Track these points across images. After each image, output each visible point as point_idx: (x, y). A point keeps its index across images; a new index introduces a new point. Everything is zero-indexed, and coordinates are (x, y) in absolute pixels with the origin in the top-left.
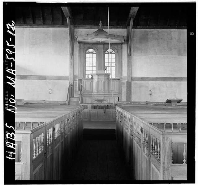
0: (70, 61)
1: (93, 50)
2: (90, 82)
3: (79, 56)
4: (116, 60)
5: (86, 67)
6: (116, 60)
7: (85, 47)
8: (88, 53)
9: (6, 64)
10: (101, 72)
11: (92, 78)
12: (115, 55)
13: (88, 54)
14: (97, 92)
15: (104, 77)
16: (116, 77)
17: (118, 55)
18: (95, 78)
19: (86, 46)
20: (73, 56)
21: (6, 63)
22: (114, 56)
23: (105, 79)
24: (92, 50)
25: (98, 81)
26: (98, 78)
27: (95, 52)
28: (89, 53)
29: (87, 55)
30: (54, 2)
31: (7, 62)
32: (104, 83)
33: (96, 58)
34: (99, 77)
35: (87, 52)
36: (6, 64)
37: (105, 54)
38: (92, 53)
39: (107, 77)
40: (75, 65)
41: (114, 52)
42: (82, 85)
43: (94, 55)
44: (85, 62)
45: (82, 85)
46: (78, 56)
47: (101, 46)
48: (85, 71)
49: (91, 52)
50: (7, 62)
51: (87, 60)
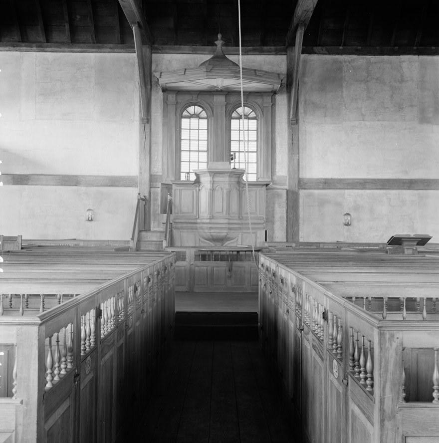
1: (201, 109)
3: (163, 125)
4: (259, 133)
7: (179, 101)
8: (186, 117)
10: (220, 166)
11: (197, 182)
12: (255, 121)
16: (260, 180)
18: (206, 180)
19: (183, 99)
20: (147, 126)
22: (253, 124)
24: (198, 109)
25: (213, 190)
26: (213, 183)
27: (204, 114)
28: (191, 116)
29: (185, 122)
32: (229, 193)
33: (208, 129)
34: (216, 179)
35: (185, 113)
37: (232, 118)
38: (197, 116)
39: (236, 180)
41: (253, 115)
42: (171, 200)
43: (204, 123)
44: (179, 139)
45: (171, 200)
46: (161, 124)
47: (221, 99)
48: (180, 132)
49: (195, 114)
51: (185, 134)
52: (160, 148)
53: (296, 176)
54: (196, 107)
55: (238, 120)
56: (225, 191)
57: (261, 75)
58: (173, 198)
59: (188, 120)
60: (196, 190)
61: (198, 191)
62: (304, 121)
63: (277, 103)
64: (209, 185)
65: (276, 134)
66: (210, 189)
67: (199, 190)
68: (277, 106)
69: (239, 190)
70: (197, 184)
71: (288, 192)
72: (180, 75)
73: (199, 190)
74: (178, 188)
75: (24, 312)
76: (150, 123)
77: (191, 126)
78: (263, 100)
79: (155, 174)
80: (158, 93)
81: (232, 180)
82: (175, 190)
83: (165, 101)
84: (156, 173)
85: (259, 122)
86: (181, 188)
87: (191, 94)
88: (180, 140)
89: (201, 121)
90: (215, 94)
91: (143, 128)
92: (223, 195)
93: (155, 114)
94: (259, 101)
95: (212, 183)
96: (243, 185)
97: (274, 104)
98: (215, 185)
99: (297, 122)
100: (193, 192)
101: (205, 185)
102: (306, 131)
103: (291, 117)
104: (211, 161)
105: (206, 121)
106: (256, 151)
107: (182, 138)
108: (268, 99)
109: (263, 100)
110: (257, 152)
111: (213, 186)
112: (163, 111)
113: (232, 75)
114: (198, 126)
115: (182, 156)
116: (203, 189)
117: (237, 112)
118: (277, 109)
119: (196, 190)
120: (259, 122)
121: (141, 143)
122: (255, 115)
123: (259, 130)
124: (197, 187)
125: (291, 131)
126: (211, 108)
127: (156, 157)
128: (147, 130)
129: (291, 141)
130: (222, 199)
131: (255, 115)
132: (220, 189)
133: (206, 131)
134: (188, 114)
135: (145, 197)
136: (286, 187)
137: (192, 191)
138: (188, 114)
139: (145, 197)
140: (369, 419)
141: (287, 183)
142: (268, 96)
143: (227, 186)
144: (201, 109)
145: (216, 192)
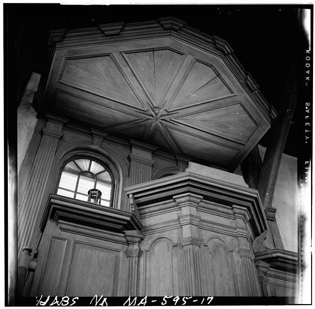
1: (101, 168)
8: (72, 172)
13: (75, 178)
19: (74, 139)
87: (92, 135)
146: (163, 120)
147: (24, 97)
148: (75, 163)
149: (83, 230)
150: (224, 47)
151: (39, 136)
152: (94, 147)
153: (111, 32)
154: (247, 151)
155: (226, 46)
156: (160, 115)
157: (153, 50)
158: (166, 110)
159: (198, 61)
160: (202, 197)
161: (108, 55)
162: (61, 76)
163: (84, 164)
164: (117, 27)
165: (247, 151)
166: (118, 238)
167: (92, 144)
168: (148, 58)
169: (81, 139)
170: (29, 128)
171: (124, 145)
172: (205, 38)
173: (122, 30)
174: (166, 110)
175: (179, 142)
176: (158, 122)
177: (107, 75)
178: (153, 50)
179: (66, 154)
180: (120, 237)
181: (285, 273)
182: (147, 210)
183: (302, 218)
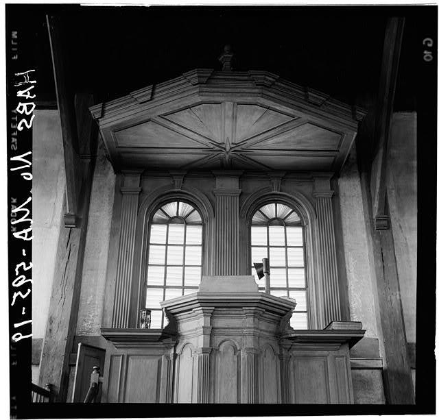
0: (59, 256)
1: (189, 208)
2: (154, 361)
3: (113, 233)
4: (310, 254)
5: (149, 292)
6: (310, 254)
7: (146, 188)
8: (161, 222)
9: (13, 49)
10: (229, 286)
11: (171, 334)
12: (300, 230)
13: (164, 228)
14: (198, 296)
15: (249, 322)
16: (335, 326)
17: (322, 225)
18: (193, 328)
19: (154, 185)
20: (77, 232)
21: (14, 46)
22: (295, 235)
23: (257, 337)
24: (185, 208)
25: (211, 352)
26: (211, 332)
27: (196, 216)
28: (170, 221)
29: (157, 233)
30: (120, 5)
31: (16, 44)
32: (256, 359)
33: (203, 245)
34: (221, 323)
35: (158, 215)
36: (13, 49)
37: (250, 224)
38: (183, 220)
39: (272, 327)
40: (85, 279)
41: (294, 217)
42: (98, 386)
43: (195, 234)
44: (143, 262)
45: (98, 386)
46: (107, 232)
47: (229, 185)
48: (147, 251)
49: (177, 217)
50: (16, 44)
51: (156, 254)
52: (102, 278)
53: (401, 337)
54: (181, 203)
55: (265, 229)
56: (244, 355)
57: (319, 102)
58: (104, 380)
59: (163, 228)
60: (168, 357)
61: (172, 358)
62: (401, 227)
63: (341, 194)
64: (201, 338)
65: (346, 250)
66: (204, 350)
67: (175, 356)
68: (342, 200)
69: (281, 356)
70: (170, 340)
71: (391, 378)
72: (141, 103)
73: (175, 356)
74: (122, 352)
75: (296, 399)
76: (82, 224)
77: (182, 272)
78: (314, 188)
79: (84, 334)
80: (106, 175)
81: (263, 328)
82: (112, 356)
83: (119, 191)
84: (87, 332)
85: (309, 231)
86: (130, 351)
87: (171, 176)
88: (146, 264)
89: (189, 229)
90: (220, 176)
91: (67, 236)
92: (239, 367)
93: (98, 214)
94: (307, 188)
95: (209, 332)
96: (290, 342)
97: (335, 196)
98: (218, 339)
99: (388, 227)
100: (160, 362)
101: (191, 341)
102: (407, 244)
103: (375, 214)
104: (209, 274)
105: (199, 230)
106: (304, 287)
107: (150, 262)
108: (323, 187)
109: (314, 188)
110: (306, 289)
111: (211, 343)
112: (114, 208)
113: (256, 91)
114: (183, 239)
115: (147, 298)
116: (187, 352)
117: (262, 213)
118: (342, 205)
119: (168, 357)
120: (309, 231)
121: (58, 265)
122: (298, 219)
123: (310, 244)
124: (168, 348)
125: (377, 242)
126: (211, 201)
127: (90, 298)
128: (76, 242)
129: (380, 264)
130: (235, 379)
131: (298, 219)
132: (231, 351)
133: (200, 249)
134: (165, 217)
135: (51, 386)
136: (383, 364)
137: (154, 361)
138: (165, 217)
139: (51, 386)
140: (23, 158)
141: (382, 354)
142: (325, 178)
143: (249, 342)
144: (191, 208)
145: (219, 359)
146: (235, 151)
147: (98, 150)
148: (163, 211)
149: (132, 346)
150: (265, 79)
151: (120, 195)
152: (176, 190)
153: (143, 99)
154: (344, 156)
155: (267, 77)
156: (228, 149)
157: (189, 107)
158: (233, 144)
159: (238, 104)
160: (213, 308)
161: (149, 120)
162: (117, 143)
163: (171, 209)
164: (147, 92)
165: (344, 156)
166: (159, 346)
167: (174, 188)
168: (188, 113)
169: (164, 182)
170: (109, 189)
171: (208, 177)
172: (241, 78)
173: (153, 94)
174: (233, 144)
175: (262, 162)
176: (230, 154)
177: (157, 133)
178: (189, 107)
179: (159, 197)
180: (160, 344)
181: (308, 353)
182: (182, 317)
183: (410, 228)
